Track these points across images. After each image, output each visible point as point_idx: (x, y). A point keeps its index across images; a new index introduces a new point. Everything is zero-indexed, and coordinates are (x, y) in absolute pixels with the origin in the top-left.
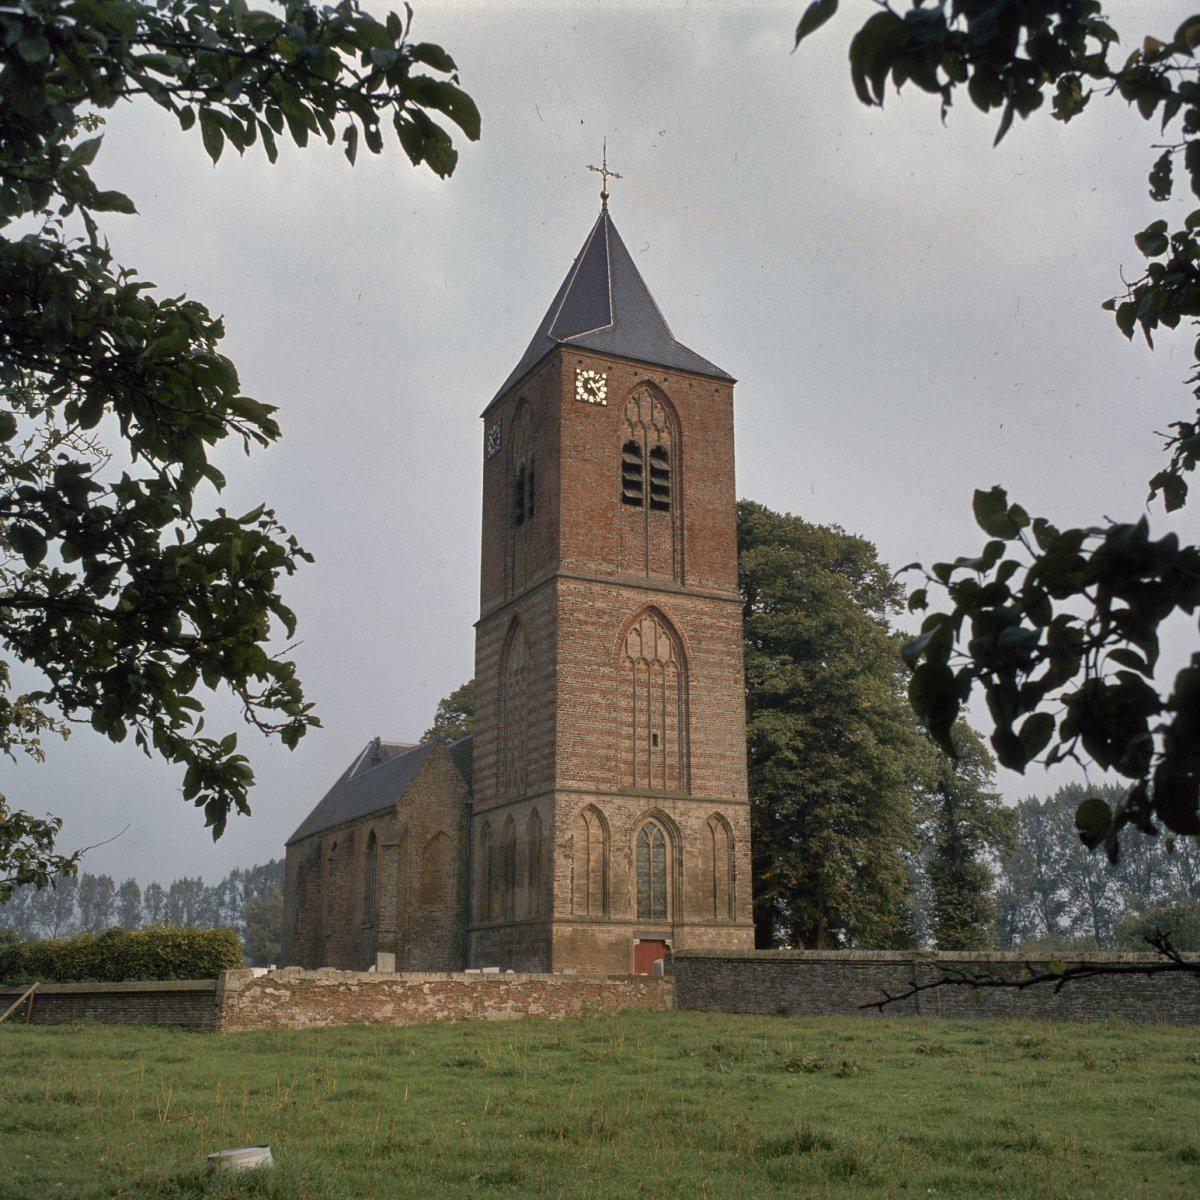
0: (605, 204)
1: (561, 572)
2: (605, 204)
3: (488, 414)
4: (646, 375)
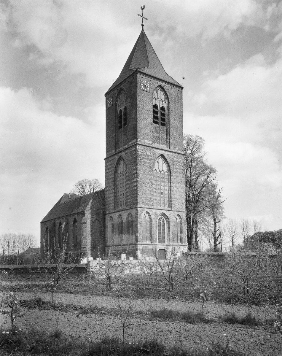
0: (143, 28)
1: (138, 143)
2: (143, 28)
3: (107, 94)
4: (160, 83)
